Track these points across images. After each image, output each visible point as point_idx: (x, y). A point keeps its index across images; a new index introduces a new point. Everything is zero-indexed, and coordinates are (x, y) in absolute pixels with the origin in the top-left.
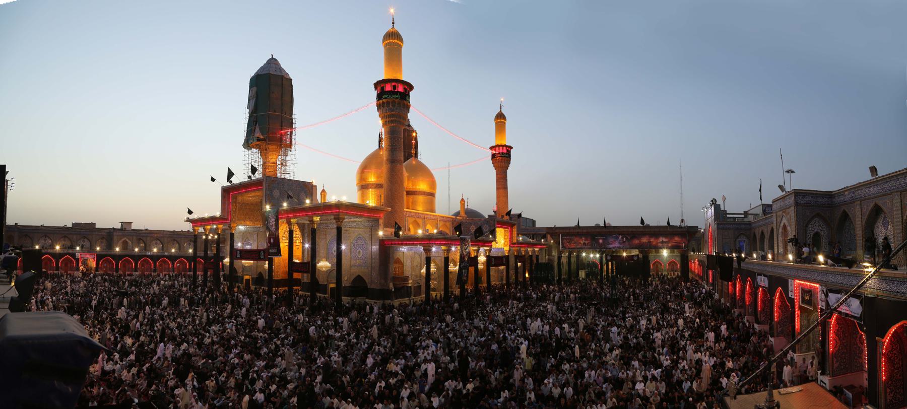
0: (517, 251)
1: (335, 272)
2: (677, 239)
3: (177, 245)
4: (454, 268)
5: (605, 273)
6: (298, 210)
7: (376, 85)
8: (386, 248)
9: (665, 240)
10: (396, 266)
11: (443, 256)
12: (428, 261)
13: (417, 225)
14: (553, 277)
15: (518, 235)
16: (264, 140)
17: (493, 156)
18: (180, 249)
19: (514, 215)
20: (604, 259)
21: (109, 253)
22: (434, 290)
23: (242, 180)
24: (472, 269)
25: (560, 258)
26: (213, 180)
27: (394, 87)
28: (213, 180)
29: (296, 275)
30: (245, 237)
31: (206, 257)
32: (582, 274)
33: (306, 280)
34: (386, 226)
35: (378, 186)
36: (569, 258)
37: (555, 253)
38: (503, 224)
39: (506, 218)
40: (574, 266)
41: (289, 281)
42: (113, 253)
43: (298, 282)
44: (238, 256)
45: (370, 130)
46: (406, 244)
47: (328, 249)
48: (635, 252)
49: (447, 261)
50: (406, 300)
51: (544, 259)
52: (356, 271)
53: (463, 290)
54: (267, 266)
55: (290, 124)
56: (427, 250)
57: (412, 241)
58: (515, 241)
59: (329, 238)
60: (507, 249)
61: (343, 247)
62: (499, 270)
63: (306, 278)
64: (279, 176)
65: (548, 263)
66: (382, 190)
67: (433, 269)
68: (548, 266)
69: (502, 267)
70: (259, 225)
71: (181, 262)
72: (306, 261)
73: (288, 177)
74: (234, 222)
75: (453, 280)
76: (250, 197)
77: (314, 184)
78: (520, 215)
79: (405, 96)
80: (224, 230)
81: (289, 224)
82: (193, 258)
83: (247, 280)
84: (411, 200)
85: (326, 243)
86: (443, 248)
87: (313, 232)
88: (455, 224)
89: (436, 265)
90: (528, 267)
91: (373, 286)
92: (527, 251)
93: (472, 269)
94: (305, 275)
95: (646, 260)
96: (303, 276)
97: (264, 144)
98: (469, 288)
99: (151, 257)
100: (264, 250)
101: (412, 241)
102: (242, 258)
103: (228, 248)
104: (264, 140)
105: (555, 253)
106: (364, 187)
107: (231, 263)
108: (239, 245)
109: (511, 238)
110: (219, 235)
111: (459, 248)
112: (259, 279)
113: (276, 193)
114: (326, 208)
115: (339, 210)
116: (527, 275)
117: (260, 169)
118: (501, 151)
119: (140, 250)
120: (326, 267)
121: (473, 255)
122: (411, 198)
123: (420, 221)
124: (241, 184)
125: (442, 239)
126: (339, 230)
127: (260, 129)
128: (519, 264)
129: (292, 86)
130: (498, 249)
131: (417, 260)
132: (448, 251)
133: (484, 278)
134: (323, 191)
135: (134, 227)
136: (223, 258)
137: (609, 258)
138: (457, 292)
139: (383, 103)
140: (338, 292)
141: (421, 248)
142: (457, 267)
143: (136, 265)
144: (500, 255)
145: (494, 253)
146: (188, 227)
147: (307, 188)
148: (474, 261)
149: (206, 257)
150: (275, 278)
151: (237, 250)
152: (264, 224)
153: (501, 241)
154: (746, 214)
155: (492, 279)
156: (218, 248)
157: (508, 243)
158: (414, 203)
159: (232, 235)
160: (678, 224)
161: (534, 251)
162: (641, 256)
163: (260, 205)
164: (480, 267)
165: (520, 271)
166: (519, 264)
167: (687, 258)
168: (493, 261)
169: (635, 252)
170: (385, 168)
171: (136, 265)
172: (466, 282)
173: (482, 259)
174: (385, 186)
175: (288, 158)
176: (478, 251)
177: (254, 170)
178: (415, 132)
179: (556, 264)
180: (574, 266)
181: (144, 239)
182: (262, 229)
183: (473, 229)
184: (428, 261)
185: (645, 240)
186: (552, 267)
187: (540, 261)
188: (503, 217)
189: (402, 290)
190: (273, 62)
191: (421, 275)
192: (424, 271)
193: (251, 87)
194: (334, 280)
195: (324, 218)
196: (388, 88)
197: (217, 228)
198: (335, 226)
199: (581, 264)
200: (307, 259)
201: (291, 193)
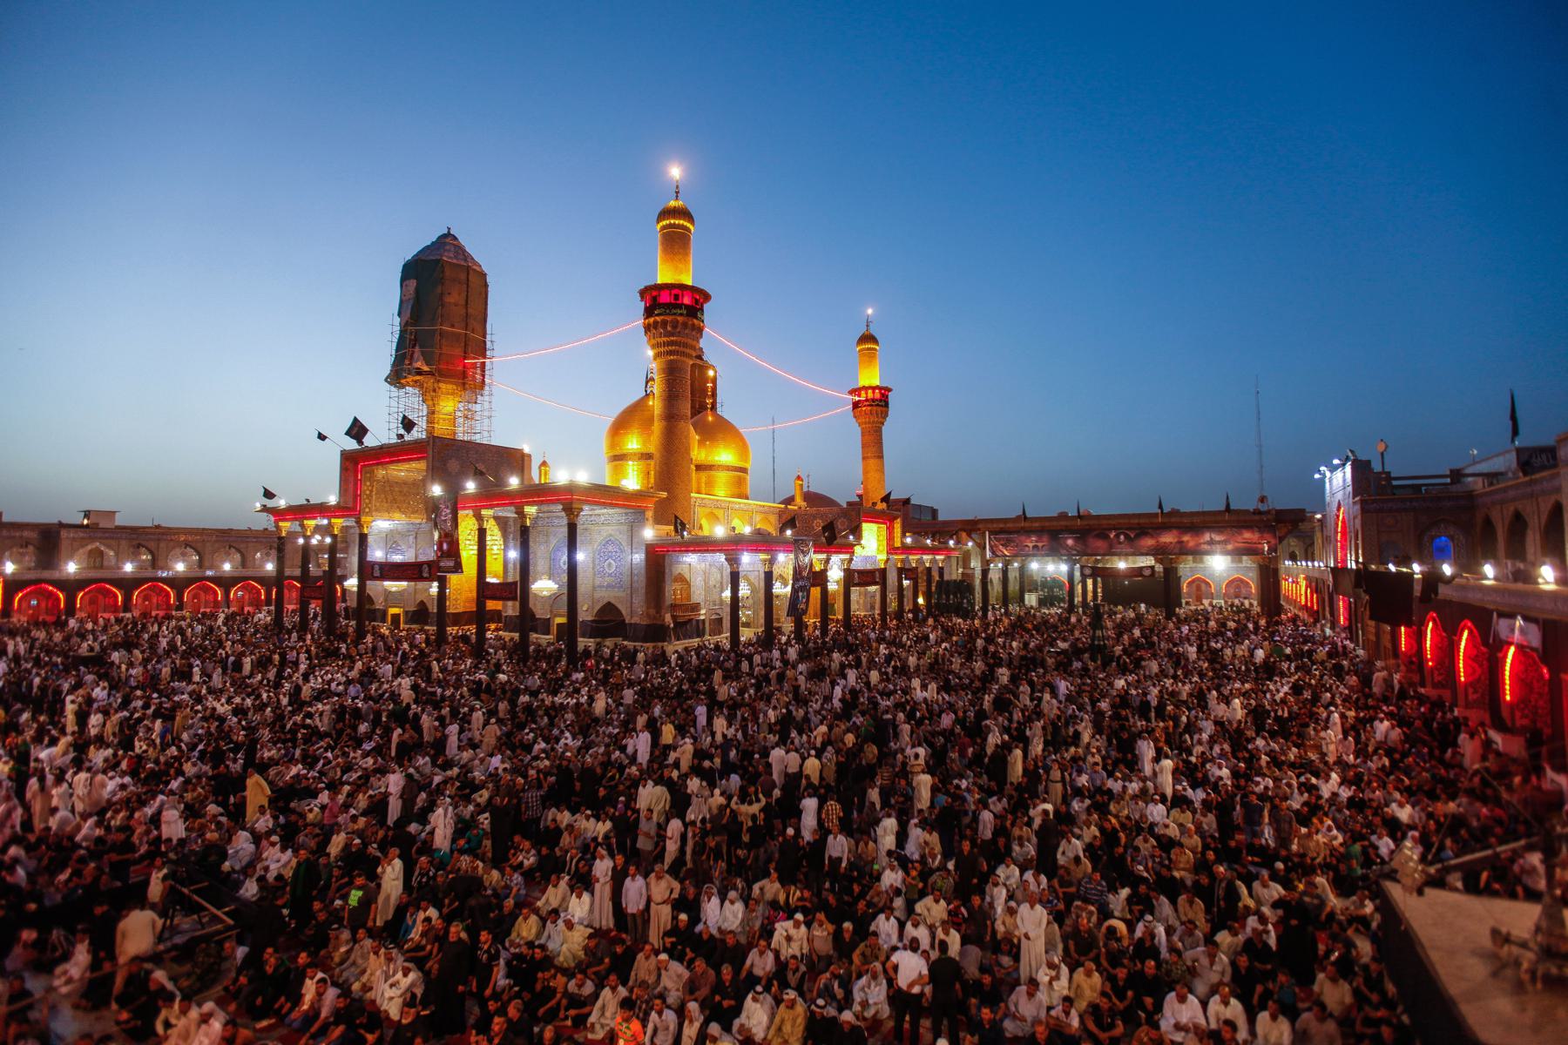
0: (903, 561)
1: (565, 598)
2: (1247, 535)
4: (782, 590)
5: (1090, 595)
6: (492, 495)
7: (643, 293)
8: (657, 560)
9: (1217, 538)
10: (677, 586)
11: (762, 569)
12: (735, 579)
13: (714, 518)
14: (973, 605)
15: (903, 535)
16: (429, 373)
17: (856, 405)
18: (244, 564)
19: (897, 501)
20: (1077, 574)
21: (46, 574)
22: (747, 625)
23: (385, 441)
24: (816, 592)
25: (985, 572)
26: (322, 437)
27: (676, 297)
28: (322, 437)
29: (491, 605)
30: (391, 540)
31: (305, 576)
32: (1031, 599)
33: (510, 612)
34: (659, 520)
35: (646, 456)
36: (1005, 572)
37: (975, 564)
38: (874, 517)
39: (882, 506)
40: (1013, 587)
41: (480, 616)
42: (63, 576)
43: (496, 616)
44: (377, 573)
45: (636, 363)
46: (694, 551)
47: (553, 560)
48: (1148, 561)
49: (769, 577)
50: (695, 642)
51: (955, 573)
52: (605, 596)
53: (800, 626)
55: (482, 350)
56: (733, 561)
57: (705, 545)
59: (553, 542)
60: (884, 557)
61: (580, 556)
62: (866, 593)
63: (511, 609)
64: (460, 437)
65: (962, 581)
66: (652, 463)
67: (744, 591)
68: (964, 587)
69: (873, 588)
70: (420, 519)
72: (510, 580)
73: (477, 439)
74: (369, 514)
76: (402, 471)
77: (527, 450)
78: (907, 501)
79: (695, 311)
80: (345, 529)
81: (479, 518)
82: (279, 580)
83: (396, 617)
84: (704, 480)
85: (548, 548)
86: (763, 556)
87: (524, 533)
88: (785, 517)
89: (750, 584)
90: (922, 587)
91: (635, 620)
92: (920, 561)
93: (816, 592)
94: (510, 603)
95: (1171, 576)
96: (505, 606)
97: (429, 382)
98: (811, 620)
99: (170, 582)
100: (429, 563)
101: (705, 545)
102: (383, 577)
103: (355, 560)
104: (429, 373)
105: (975, 564)
106: (619, 458)
107: (362, 586)
108: (377, 554)
109: (890, 538)
110: (334, 537)
111: (792, 556)
112: (419, 614)
114: (542, 493)
115: (569, 501)
116: (921, 601)
117: (422, 424)
119: (189, 567)
121: (818, 568)
122: (703, 475)
123: (720, 513)
124: (381, 447)
125: (762, 542)
127: (423, 354)
128: (906, 583)
129: (486, 286)
130: (866, 558)
131: (715, 577)
132: (772, 562)
133: (839, 606)
134: (544, 464)
135: (120, 521)
136: (344, 578)
137: (1088, 572)
138: (788, 626)
139: (656, 323)
140: (569, 631)
141: (721, 557)
142: (789, 589)
143: (180, 597)
144: (869, 567)
145: (857, 564)
146: (266, 522)
147: (515, 459)
148: (820, 578)
149: (305, 576)
150: (451, 610)
151: (373, 564)
152: (429, 519)
153: (872, 545)
155: (854, 606)
156: (333, 562)
157: (884, 547)
159: (363, 539)
160: (1251, 505)
161: (934, 561)
162: (1159, 568)
163: (420, 486)
164: (832, 587)
165: (908, 594)
166: (906, 583)
167: (1276, 572)
168: (854, 578)
169: (1148, 561)
170: (657, 427)
171: (180, 597)
172: (805, 612)
173: (835, 575)
174: (657, 455)
175: (477, 407)
176: (827, 561)
177: (408, 424)
178: (713, 367)
179: (977, 582)
182: (426, 526)
183: (818, 525)
184: (735, 579)
185: (1168, 538)
188: (874, 504)
189: (688, 625)
190: (447, 241)
191: (722, 602)
192: (727, 594)
193: (403, 280)
194: (564, 610)
195: (544, 508)
196: (665, 298)
197: (330, 525)
199: (1027, 583)
200: (514, 576)
201: (481, 467)
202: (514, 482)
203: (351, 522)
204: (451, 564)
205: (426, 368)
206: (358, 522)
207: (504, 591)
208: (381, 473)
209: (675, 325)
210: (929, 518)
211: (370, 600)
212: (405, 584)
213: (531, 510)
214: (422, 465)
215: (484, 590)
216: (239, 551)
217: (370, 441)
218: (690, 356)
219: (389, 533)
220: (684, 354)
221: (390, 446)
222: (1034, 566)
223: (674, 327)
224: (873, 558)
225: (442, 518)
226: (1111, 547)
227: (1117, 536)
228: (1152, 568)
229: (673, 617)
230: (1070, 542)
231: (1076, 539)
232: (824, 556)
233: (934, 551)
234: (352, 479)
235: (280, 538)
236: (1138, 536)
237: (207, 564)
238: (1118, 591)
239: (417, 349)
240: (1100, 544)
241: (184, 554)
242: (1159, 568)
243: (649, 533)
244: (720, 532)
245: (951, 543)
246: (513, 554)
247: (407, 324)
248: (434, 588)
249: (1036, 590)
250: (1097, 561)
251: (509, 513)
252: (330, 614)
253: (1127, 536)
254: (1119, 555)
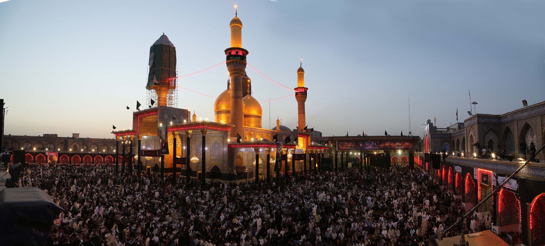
0: (311, 151)
1: (201, 164)
2: (407, 144)
3: (106, 148)
4: (273, 161)
5: (363, 164)
6: (179, 126)
7: (226, 51)
8: (232, 149)
9: (400, 144)
10: (238, 160)
11: (266, 154)
12: (257, 157)
13: (251, 135)
14: (332, 167)
15: (311, 141)
16: (159, 84)
17: (296, 94)
18: (108, 150)
19: (309, 129)
20: (363, 156)
21: (66, 152)
22: (261, 174)
23: (146, 108)
24: (283, 162)
25: (336, 155)
26: (128, 108)
27: (237, 52)
28: (128, 108)
29: (178, 166)
30: (147, 142)
31: (124, 155)
32: (350, 165)
33: (184, 168)
34: (232, 136)
35: (227, 112)
36: (342, 155)
37: (333, 152)
38: (302, 135)
39: (304, 131)
40: (345, 160)
41: (174, 169)
42: (68, 152)
43: (179, 170)
44: (143, 154)
46: (244, 147)
47: (197, 150)
48: (382, 152)
49: (268, 157)
50: (244, 181)
51: (327, 156)
52: (214, 163)
53: (278, 174)
54: (160, 160)
55: (174, 75)
56: (257, 151)
57: (248, 145)
58: (309, 145)
59: (198, 143)
60: (304, 150)
61: (206, 149)
62: (300, 162)
63: (184, 167)
64: (168, 106)
65: (329, 158)
66: (230, 114)
67: (260, 162)
68: (330, 160)
69: (302, 161)
70: (155, 135)
71: (108, 158)
72: (184, 157)
73: (173, 106)
74: (141, 134)
75: (272, 168)
76: (150, 118)
77: (189, 110)
78: (312, 129)
79: (243, 58)
80: (134, 139)
81: (174, 134)
82: (116, 155)
83: (149, 169)
84: (247, 120)
85: (196, 146)
86: (266, 149)
87: (188, 140)
88: (274, 135)
89: (262, 159)
90: (317, 161)
91: (224, 172)
92: (316, 151)
93: (283, 162)
94: (183, 165)
95: (388, 156)
96: (182, 166)
97: (158, 87)
98: (282, 173)
99: (91, 155)
100: (158, 151)
101: (248, 145)
102: (145, 155)
103: (137, 149)
104: (159, 84)
105: (333, 152)
106: (219, 113)
107: (139, 158)
108: (143, 147)
109: (307, 143)
110: (131, 141)
111: (276, 149)
112: (156, 168)
113: (166, 116)
115: (204, 127)
116: (317, 166)
117: (156, 102)
118: (301, 91)
119: (84, 151)
120: (196, 161)
121: (284, 153)
122: (247, 119)
123: (252, 133)
124: (145, 111)
125: (266, 144)
126: (204, 138)
127: (156, 77)
128: (312, 159)
129: (175, 52)
130: (299, 150)
131: (251, 156)
132: (269, 151)
133: (291, 167)
134: (194, 115)
135: (80, 136)
136: (134, 155)
137: (366, 155)
138: (275, 175)
139: (230, 62)
140: (203, 176)
141: (253, 149)
142: (275, 161)
143: (82, 159)
144: (300, 153)
145: (297, 152)
146: (113, 137)
147: (185, 113)
148: (285, 157)
149: (124, 155)
150: (165, 167)
151: (142, 150)
152: (159, 135)
153: (301, 145)
155: (296, 168)
156: (131, 149)
157: (305, 146)
158: (249, 122)
159: (139, 141)
160: (407, 134)
161: (321, 151)
162: (385, 154)
163: (156, 123)
164: (289, 160)
165: (313, 163)
166: (312, 159)
167: (413, 155)
168: (296, 157)
169: (382, 152)
170: (231, 101)
171: (82, 159)
172: (280, 170)
173: (290, 156)
174: (231, 112)
175: (173, 95)
176: (287, 151)
177: (152, 102)
178: (249, 79)
179: (334, 159)
180: (345, 160)
181: (87, 144)
182: (158, 138)
183: (284, 138)
184: (257, 157)
185: (387, 144)
186: (332, 161)
187: (324, 157)
188: (302, 130)
189: (242, 174)
190: (164, 37)
191: (253, 165)
192: (255, 163)
193: (151, 52)
194: (201, 168)
195: (195, 131)
196: (233, 53)
197: (130, 137)
198: (201, 136)
199: (349, 159)
200: (184, 156)
201: (175, 116)
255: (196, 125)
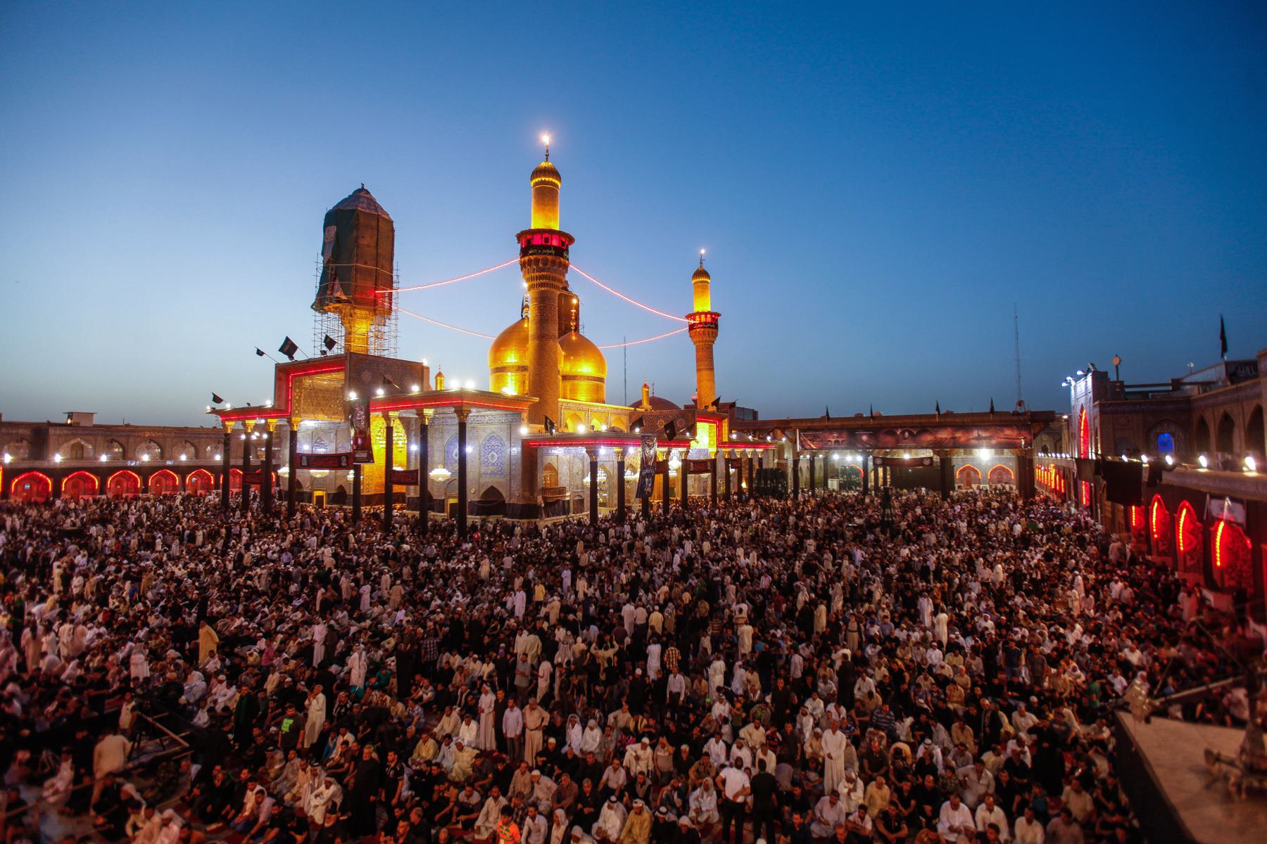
0: (729, 453)
1: (457, 483)
2: (1008, 432)
4: (632, 476)
5: (881, 480)
6: (398, 400)
7: (519, 237)
8: (531, 452)
9: (984, 434)
10: (547, 473)
11: (615, 460)
12: (594, 468)
13: (577, 418)
14: (786, 489)
15: (730, 432)
16: (347, 302)
17: (691, 327)
18: (197, 455)
19: (725, 405)
20: (870, 464)
21: (37, 464)
22: (604, 505)
23: (311, 356)
24: (659, 478)
25: (796, 462)
26: (260, 353)
27: (547, 240)
28: (260, 353)
29: (397, 489)
30: (316, 436)
31: (246, 465)
32: (833, 484)
33: (412, 495)
34: (532, 420)
35: (522, 369)
36: (812, 462)
37: (788, 455)
38: (707, 417)
39: (712, 409)
40: (819, 474)
41: (388, 498)
42: (51, 465)
43: (401, 497)
44: (305, 463)
46: (561, 445)
47: (447, 452)
48: (928, 453)
49: (621, 466)
50: (562, 518)
51: (771, 463)
52: (489, 481)
53: (646, 505)
55: (389, 283)
56: (592, 453)
57: (569, 441)
59: (447, 437)
60: (714, 450)
61: (469, 449)
62: (700, 479)
63: (413, 492)
64: (372, 353)
65: (777, 470)
66: (527, 374)
67: (601, 477)
68: (779, 474)
69: (705, 475)
70: (339, 419)
72: (412, 468)
73: (386, 354)
74: (299, 415)
76: (325, 381)
77: (426, 363)
78: (733, 405)
79: (561, 251)
80: (279, 427)
81: (387, 418)
82: (225, 469)
83: (320, 499)
84: (568, 387)
85: (443, 442)
86: (617, 449)
87: (424, 430)
88: (635, 418)
89: (606, 471)
90: (745, 474)
91: (513, 501)
92: (743, 453)
93: (659, 478)
94: (412, 487)
95: (946, 465)
96: (408, 490)
97: (347, 309)
98: (655, 501)
99: (138, 470)
100: (347, 455)
101: (569, 441)
102: (310, 466)
103: (287, 452)
104: (347, 302)
105: (788, 455)
106: (500, 370)
107: (292, 473)
108: (305, 448)
109: (719, 435)
110: (270, 433)
111: (640, 449)
112: (339, 496)
115: (460, 404)
116: (744, 485)
117: (341, 342)
119: (153, 458)
121: (661, 458)
122: (568, 384)
123: (582, 414)
124: (308, 361)
125: (615, 438)
127: (342, 286)
128: (732, 471)
129: (393, 231)
130: (700, 451)
131: (578, 466)
132: (623, 454)
133: (678, 489)
134: (440, 374)
135: (97, 421)
136: (278, 467)
137: (879, 462)
138: (636, 505)
139: (530, 261)
140: (460, 510)
141: (583, 450)
142: (637, 475)
143: (145, 482)
144: (702, 458)
145: (693, 456)
146: (215, 421)
147: (416, 371)
148: (663, 467)
149: (246, 465)
150: (364, 493)
151: (301, 456)
152: (347, 419)
153: (704, 440)
154: (1177, 384)
155: (690, 490)
156: (269, 454)
157: (714, 442)
159: (293, 435)
160: (1011, 408)
161: (754, 453)
162: (937, 459)
163: (339, 392)
164: (672, 474)
165: (734, 480)
166: (732, 471)
167: (1031, 462)
168: (690, 467)
169: (928, 453)
170: (531, 345)
171: (145, 482)
172: (650, 494)
173: (675, 464)
174: (531, 368)
175: (386, 329)
176: (668, 453)
177: (330, 343)
178: (577, 297)
179: (790, 470)
182: (344, 425)
183: (661, 424)
184: (594, 468)
185: (944, 435)
188: (706, 407)
189: (556, 505)
190: (361, 194)
191: (583, 486)
192: (588, 480)
193: (326, 226)
194: (456, 492)
195: (440, 410)
196: (538, 241)
197: (267, 424)
199: (829, 471)
200: (415, 465)
201: (388, 377)
202: (415, 389)
203: (284, 422)
204: (365, 455)
205: (344, 298)
206: (290, 421)
207: (408, 477)
208: (308, 382)
209: (545, 262)
210: (751, 418)
211: (299, 485)
212: (327, 471)
213: (429, 412)
214: (341, 376)
215: (391, 476)
216: (193, 445)
217: (299, 356)
218: (557, 288)
219: (314, 431)
220: (552, 286)
221: (315, 360)
222: (836, 457)
223: (545, 264)
224: (705, 451)
225: (358, 418)
226: (898, 442)
227: (903, 433)
228: (931, 458)
229: (544, 498)
230: (865, 438)
231: (869, 436)
232: (665, 449)
233: (754, 445)
234: (284, 387)
235: (227, 435)
236: (919, 433)
237: (167, 455)
238: (903, 477)
239: (337, 282)
240: (889, 439)
241: (148, 448)
242: (937, 459)
243: (524, 431)
244: (582, 429)
245: (769, 438)
246: (415, 448)
247: (329, 262)
248: (351, 475)
249: (837, 476)
250: (887, 453)
251: (411, 414)
252: (266, 496)
253: (910, 433)
254: (904, 448)
255: (438, 398)
